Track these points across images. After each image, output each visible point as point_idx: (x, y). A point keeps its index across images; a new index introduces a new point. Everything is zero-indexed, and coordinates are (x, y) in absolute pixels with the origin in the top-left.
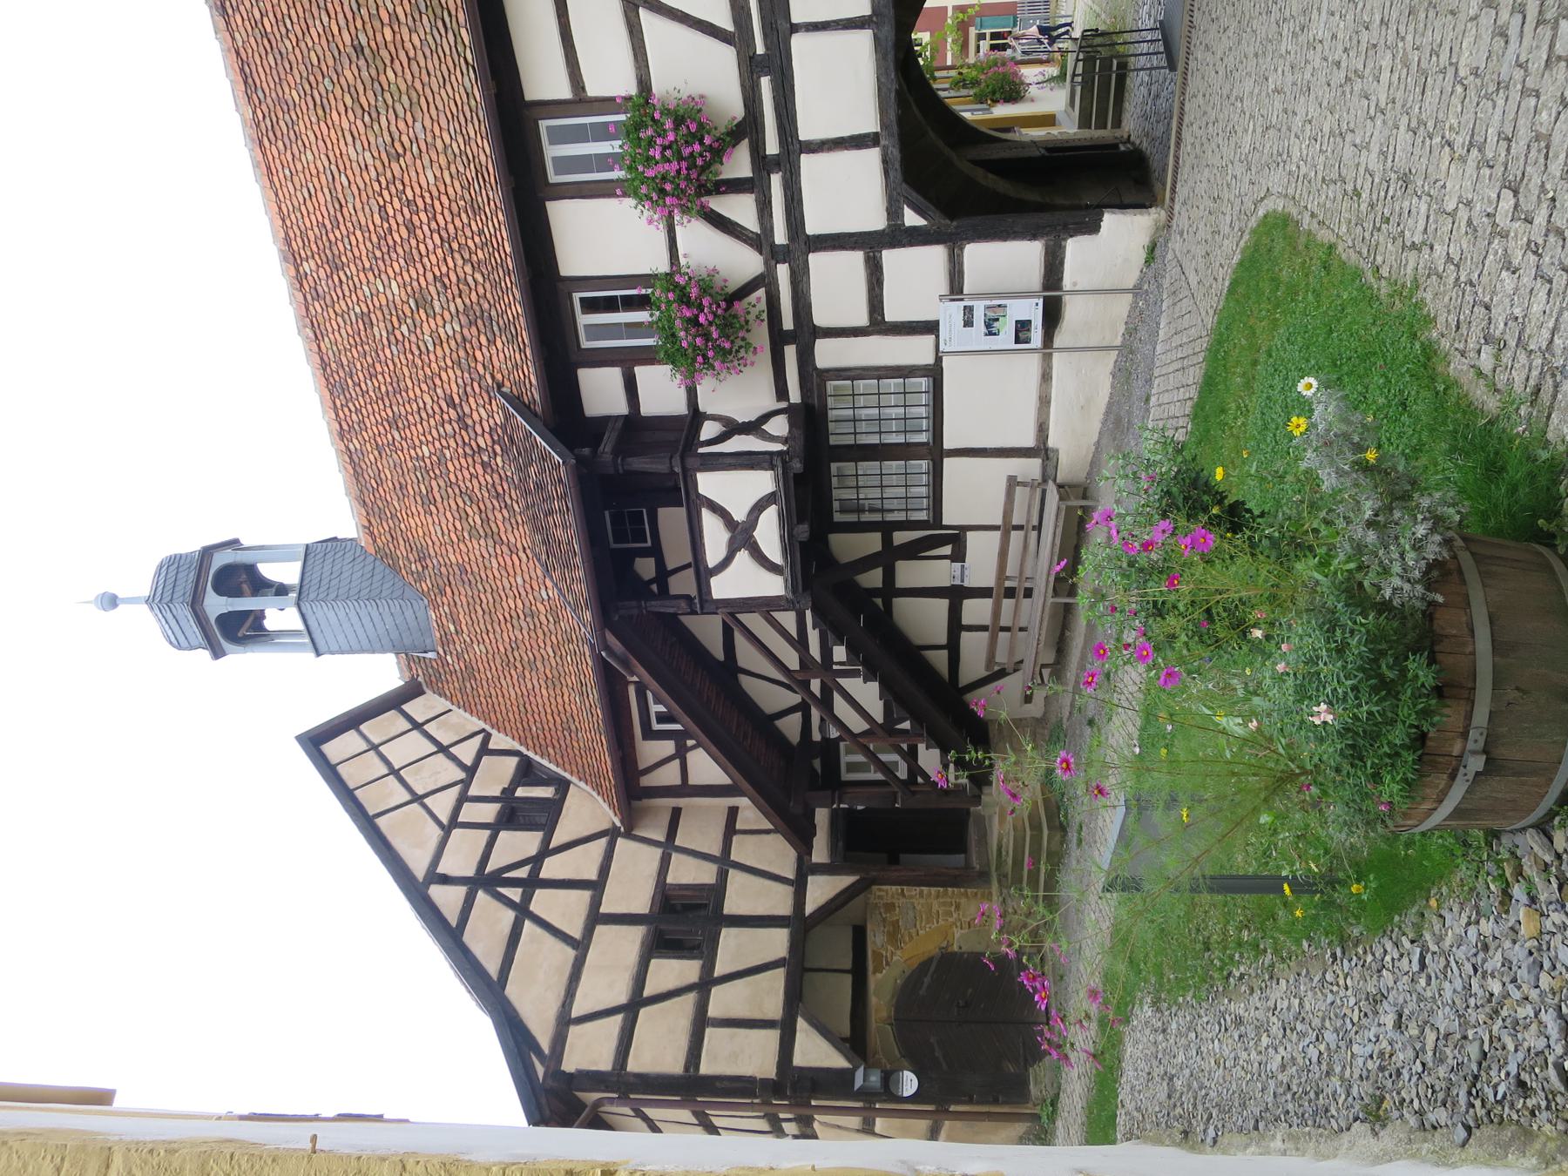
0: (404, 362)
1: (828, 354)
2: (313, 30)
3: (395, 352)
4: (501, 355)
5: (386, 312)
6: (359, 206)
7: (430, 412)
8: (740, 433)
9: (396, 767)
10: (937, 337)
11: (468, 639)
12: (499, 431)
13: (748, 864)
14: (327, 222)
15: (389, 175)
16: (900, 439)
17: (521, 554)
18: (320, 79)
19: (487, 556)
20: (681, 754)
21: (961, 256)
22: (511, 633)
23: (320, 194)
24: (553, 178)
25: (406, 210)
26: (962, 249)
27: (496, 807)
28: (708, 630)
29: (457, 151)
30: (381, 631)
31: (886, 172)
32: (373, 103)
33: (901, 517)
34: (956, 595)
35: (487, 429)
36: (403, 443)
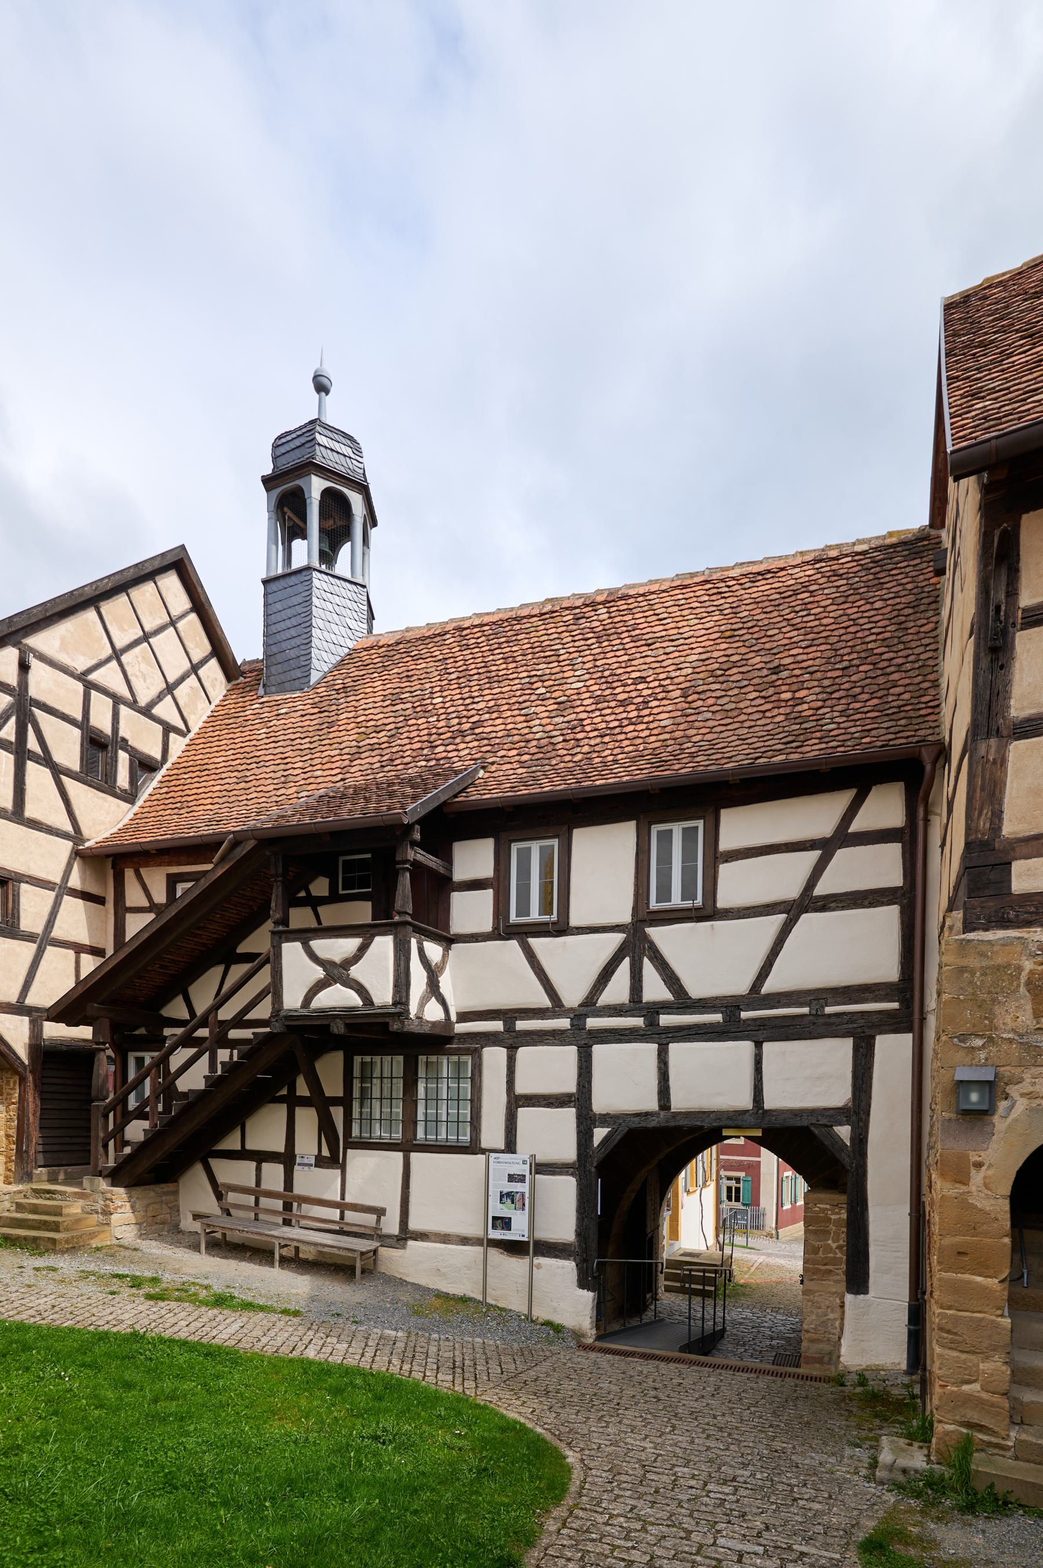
0: (514, 688)
1: (494, 1057)
2: (795, 633)
3: (523, 681)
4: (511, 772)
5: (558, 676)
6: (648, 660)
7: (470, 707)
8: (429, 977)
9: (151, 640)
10: (502, 1152)
11: (271, 724)
12: (447, 765)
13: (43, 962)
14: (637, 632)
15: (671, 688)
16: (420, 1116)
17: (340, 777)
18: (755, 636)
19: (342, 746)
20: (153, 907)
21: (567, 1174)
22: (272, 762)
23: (661, 628)
24: (655, 829)
25: (640, 699)
26: (572, 1175)
27: (108, 730)
28: (258, 942)
29: (685, 746)
30: (284, 645)
31: (638, 1115)
32: (732, 679)
33: (356, 1114)
34: (288, 1159)
35: (450, 755)
36: (446, 682)
